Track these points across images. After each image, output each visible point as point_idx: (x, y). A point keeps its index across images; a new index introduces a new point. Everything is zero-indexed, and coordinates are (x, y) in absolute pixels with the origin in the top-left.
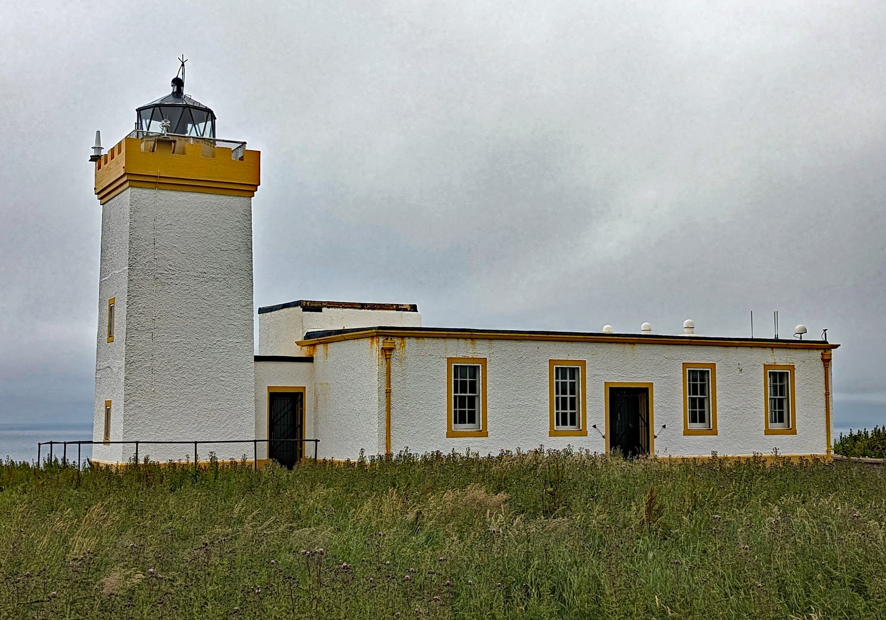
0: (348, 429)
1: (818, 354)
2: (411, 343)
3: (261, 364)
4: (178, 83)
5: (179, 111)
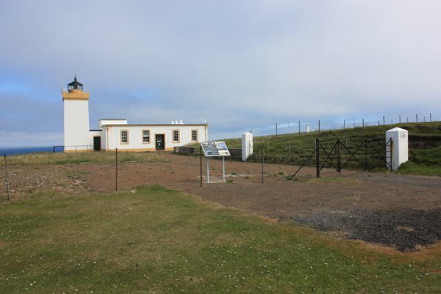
2: (113, 128)
4: (75, 79)
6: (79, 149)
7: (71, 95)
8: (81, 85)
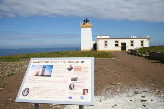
4: (86, 19)
7: (84, 26)
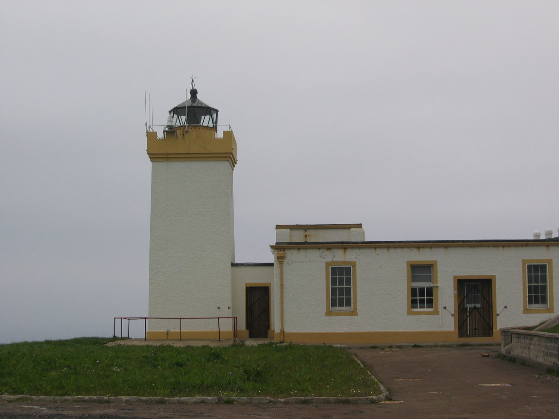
0: (302, 313)
1: (236, 261)
3: (235, 268)
4: (194, 93)
5: (194, 111)
6: (189, 327)
8: (209, 111)
